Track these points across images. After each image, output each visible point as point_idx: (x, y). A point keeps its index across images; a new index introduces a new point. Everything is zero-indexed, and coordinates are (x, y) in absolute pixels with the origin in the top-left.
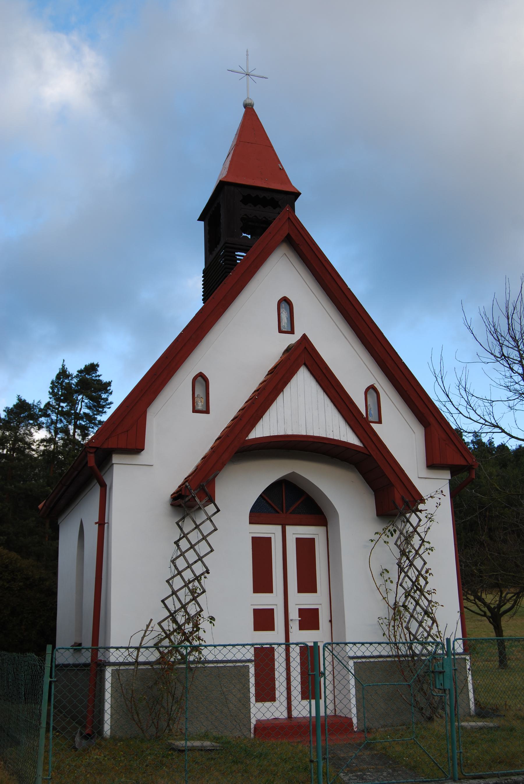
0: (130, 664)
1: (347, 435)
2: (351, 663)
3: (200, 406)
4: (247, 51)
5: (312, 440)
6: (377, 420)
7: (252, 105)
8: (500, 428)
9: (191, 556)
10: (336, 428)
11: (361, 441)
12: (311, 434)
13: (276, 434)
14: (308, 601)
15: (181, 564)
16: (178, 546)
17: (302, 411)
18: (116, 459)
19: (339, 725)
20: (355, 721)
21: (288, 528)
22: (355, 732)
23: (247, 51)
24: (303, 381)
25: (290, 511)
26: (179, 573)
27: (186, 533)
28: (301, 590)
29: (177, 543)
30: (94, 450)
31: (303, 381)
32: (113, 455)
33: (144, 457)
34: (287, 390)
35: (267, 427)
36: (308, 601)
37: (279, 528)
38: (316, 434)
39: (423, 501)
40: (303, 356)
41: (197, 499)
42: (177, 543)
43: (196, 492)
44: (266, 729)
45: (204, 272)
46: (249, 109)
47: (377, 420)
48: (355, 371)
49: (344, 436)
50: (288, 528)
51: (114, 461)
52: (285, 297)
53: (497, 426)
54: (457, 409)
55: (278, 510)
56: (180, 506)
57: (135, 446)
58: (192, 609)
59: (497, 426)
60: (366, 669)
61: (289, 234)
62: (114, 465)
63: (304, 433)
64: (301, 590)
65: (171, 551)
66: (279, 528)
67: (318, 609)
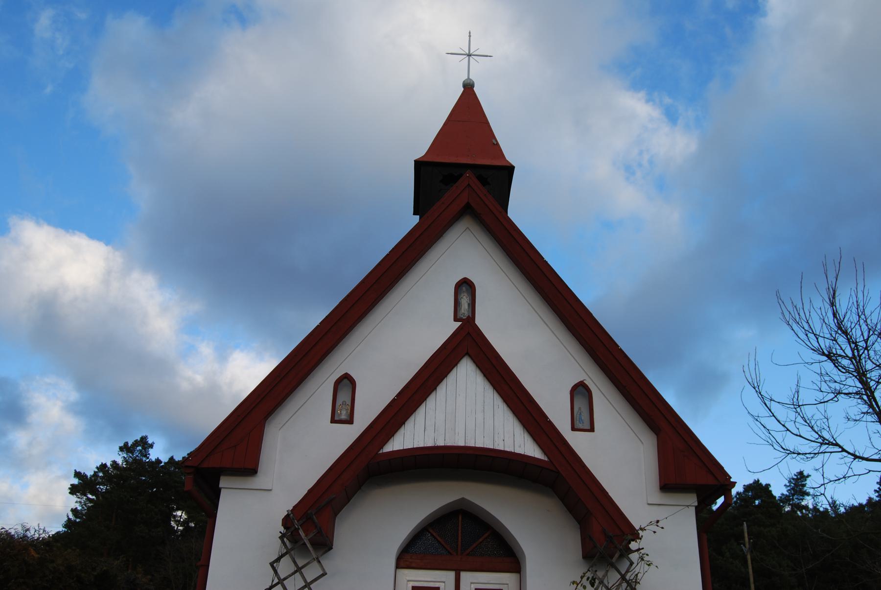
1: (525, 446)
3: (344, 416)
6: (588, 427)
8: (840, 447)
10: (511, 438)
11: (545, 454)
12: (471, 444)
13: (422, 445)
17: (465, 415)
24: (466, 377)
27: (282, 578)
31: (466, 377)
32: (222, 478)
33: (260, 480)
35: (412, 436)
37: (451, 575)
38: (479, 445)
39: (635, 535)
40: (467, 343)
41: (301, 533)
43: (301, 522)
46: (468, 87)
47: (588, 427)
48: (547, 364)
49: (520, 447)
52: (465, 278)
53: (837, 445)
54: (784, 425)
57: (248, 467)
59: (837, 445)
62: (222, 491)
63: (462, 444)
66: (451, 575)
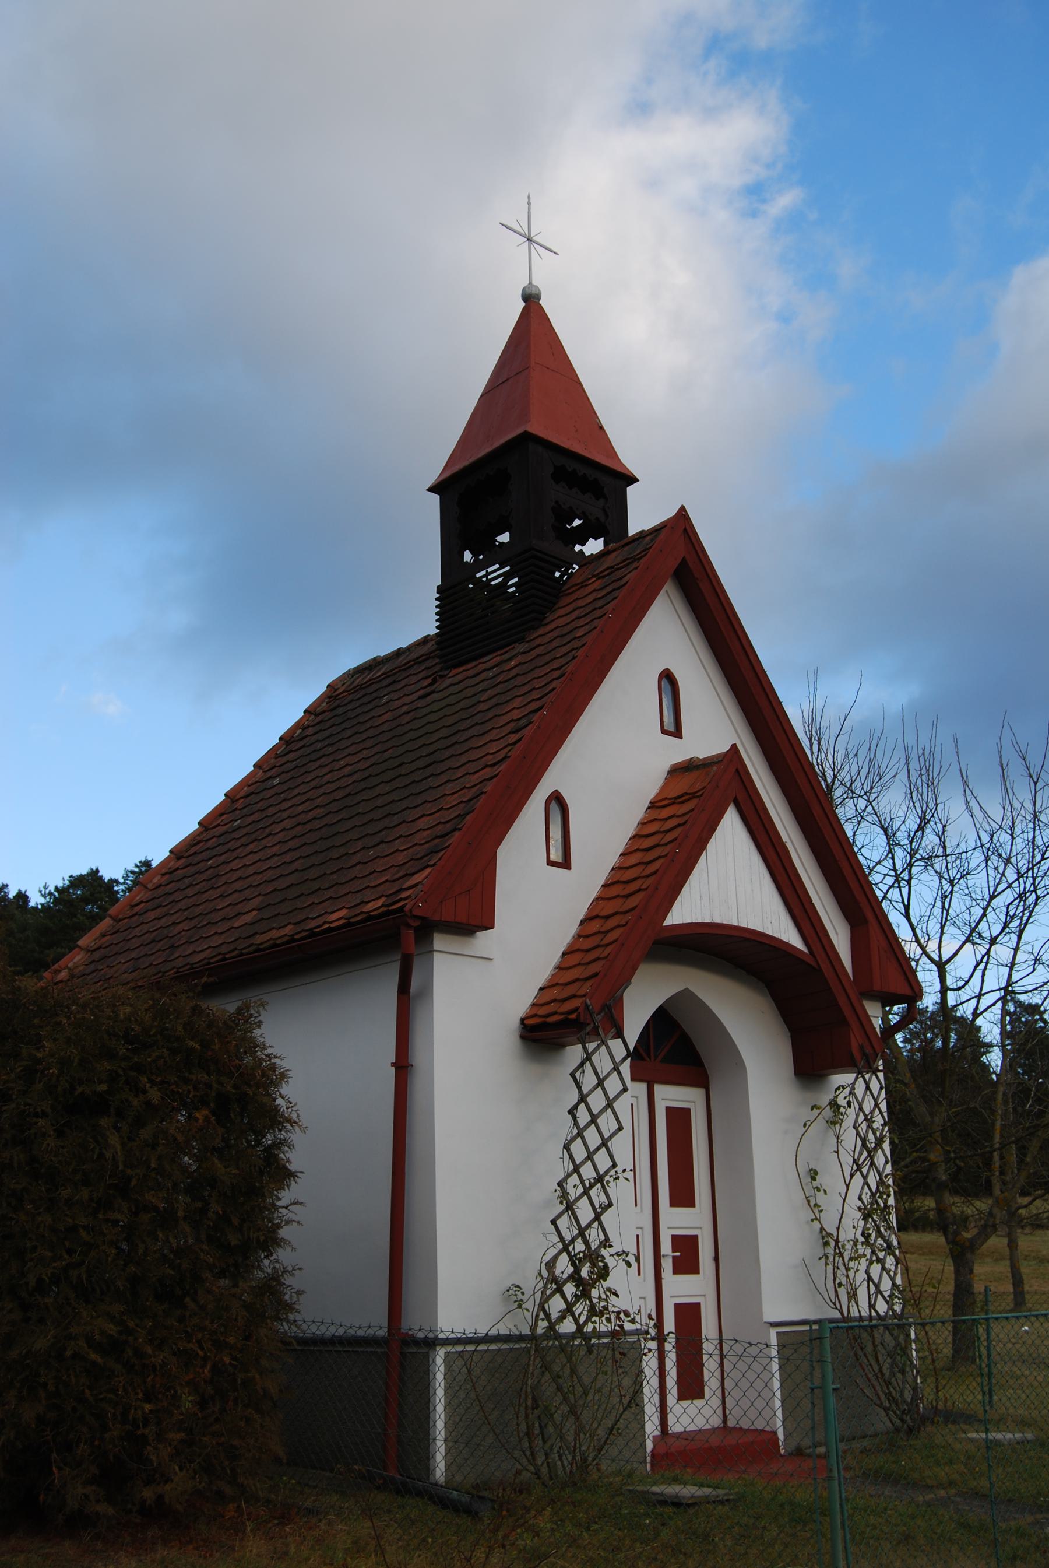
0: (521, 1338)
2: (773, 1332)
4: (529, 197)
5: (747, 936)
7: (538, 297)
9: (592, 1138)
13: (707, 920)
14: (677, 1221)
15: (578, 1151)
16: (574, 1118)
18: (439, 942)
19: (757, 1446)
20: (781, 1435)
21: (658, 1089)
22: (781, 1456)
23: (529, 197)
25: (660, 1057)
26: (576, 1169)
28: (674, 1203)
29: (572, 1112)
30: (416, 924)
32: (435, 935)
34: (711, 846)
36: (677, 1221)
38: (751, 927)
42: (572, 1112)
44: (679, 1453)
45: (439, 590)
50: (658, 1089)
51: (437, 945)
55: (644, 1054)
56: (534, 1041)
58: (595, 1235)
60: (803, 1344)
61: (684, 559)
62: (435, 954)
64: (674, 1203)
65: (565, 1128)
67: (696, 1236)
